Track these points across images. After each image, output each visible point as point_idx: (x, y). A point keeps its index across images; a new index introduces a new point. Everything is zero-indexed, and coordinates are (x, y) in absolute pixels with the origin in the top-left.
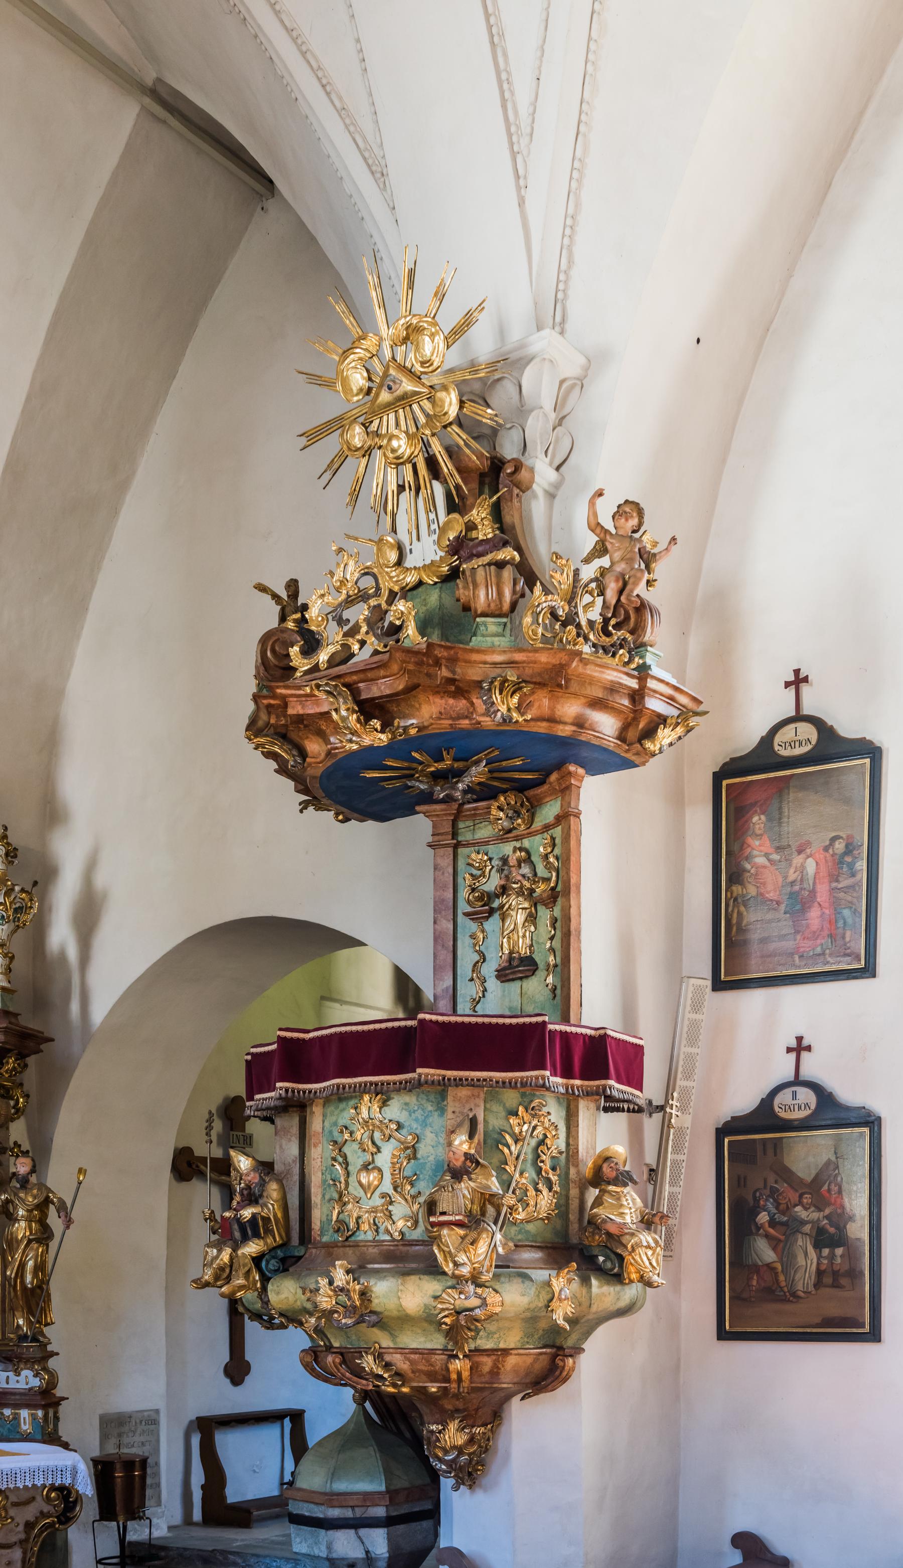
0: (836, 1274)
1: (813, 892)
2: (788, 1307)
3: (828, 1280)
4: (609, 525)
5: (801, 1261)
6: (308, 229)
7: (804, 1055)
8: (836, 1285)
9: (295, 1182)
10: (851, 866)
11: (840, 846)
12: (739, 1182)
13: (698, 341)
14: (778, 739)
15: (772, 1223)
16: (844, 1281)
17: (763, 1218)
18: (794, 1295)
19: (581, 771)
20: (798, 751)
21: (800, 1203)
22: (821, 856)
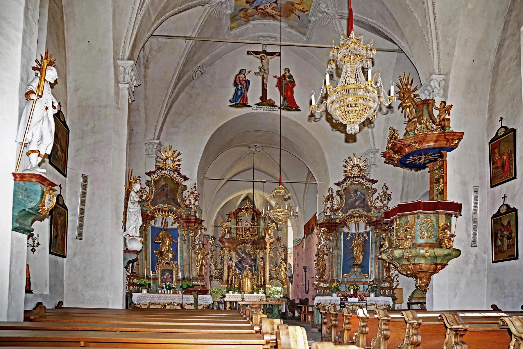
0: (510, 245)
1: (506, 163)
2: (503, 254)
3: (509, 247)
4: (439, 107)
5: (505, 243)
6: (14, 197)
7: (505, 198)
8: (511, 248)
9: (70, 247)
10: (511, 155)
11: (509, 152)
12: (495, 228)
13: (473, 61)
14: (499, 132)
15: (500, 236)
16: (512, 247)
17: (499, 235)
18: (504, 251)
19: (445, 152)
20: (502, 134)
21: (505, 231)
22: (506, 155)
